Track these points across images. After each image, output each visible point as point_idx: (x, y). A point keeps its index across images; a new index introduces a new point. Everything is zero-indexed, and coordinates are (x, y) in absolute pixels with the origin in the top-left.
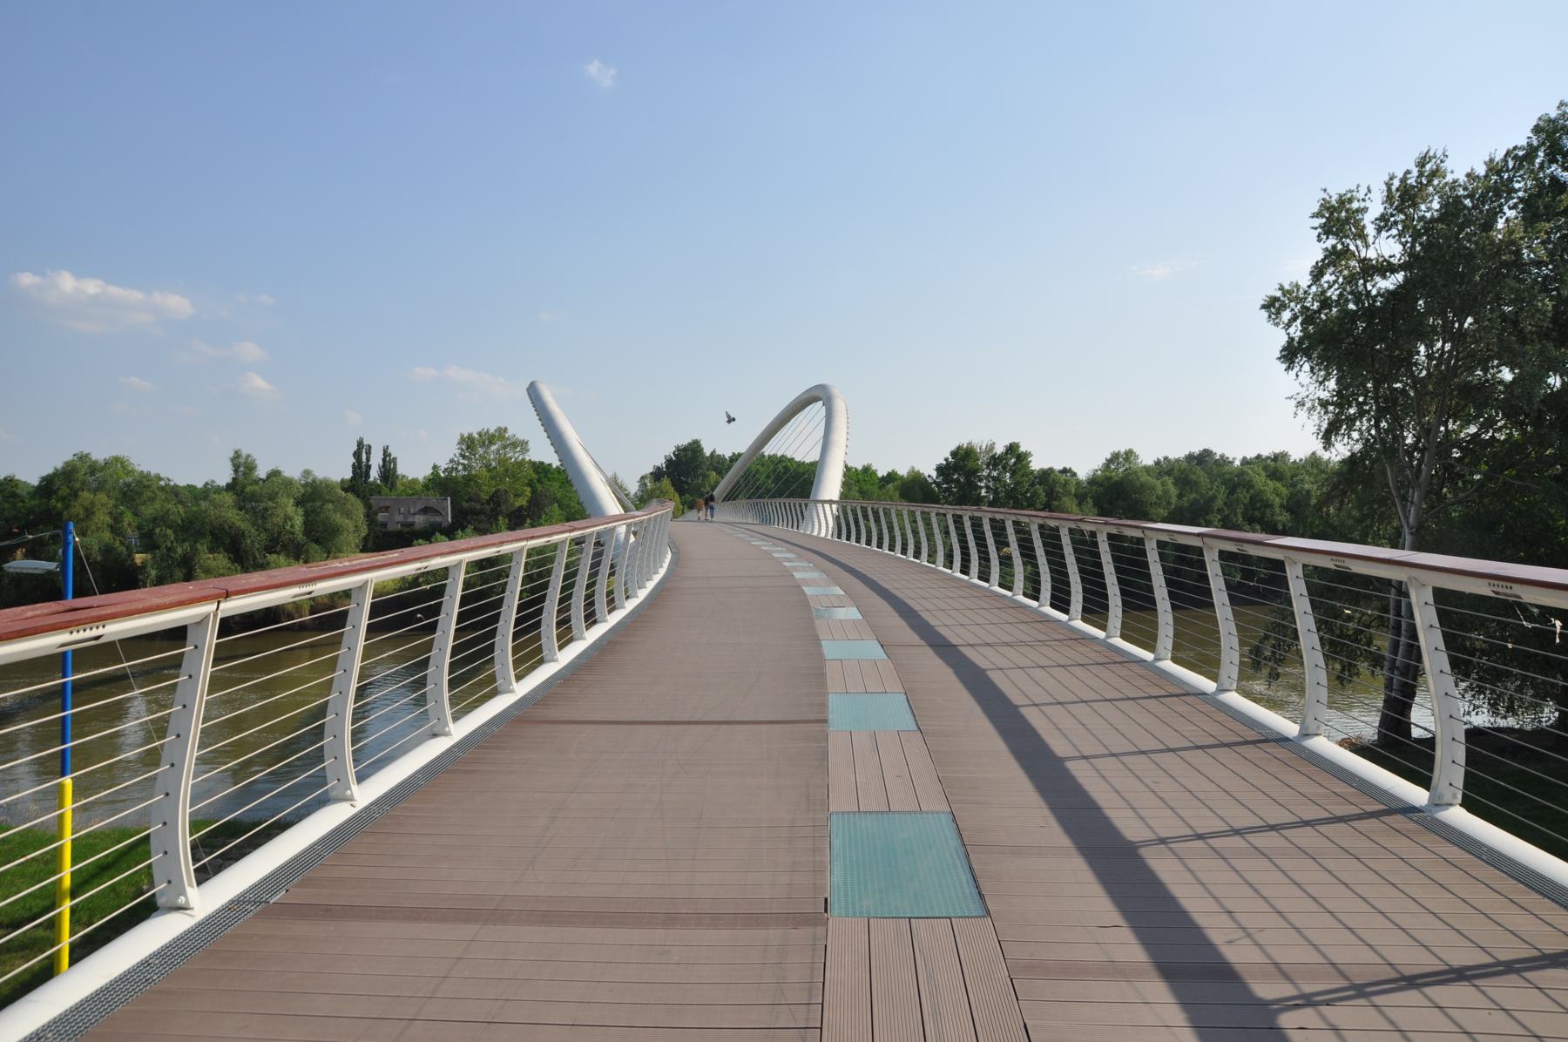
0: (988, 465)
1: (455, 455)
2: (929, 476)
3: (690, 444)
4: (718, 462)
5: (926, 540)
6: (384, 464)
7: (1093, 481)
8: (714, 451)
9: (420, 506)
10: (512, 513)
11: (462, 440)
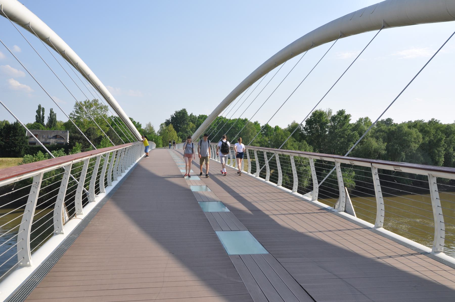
1: (73, 111)
3: (181, 111)
4: (193, 118)
6: (50, 116)
8: (192, 114)
9: (53, 135)
10: (96, 139)
11: (77, 105)
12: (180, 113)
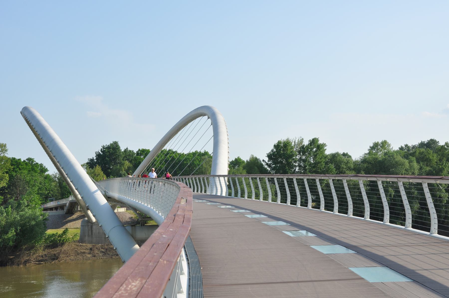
0: (299, 152)
2: (263, 161)
3: (111, 145)
5: (349, 192)
7: (364, 161)
8: (127, 149)
12: (108, 148)
